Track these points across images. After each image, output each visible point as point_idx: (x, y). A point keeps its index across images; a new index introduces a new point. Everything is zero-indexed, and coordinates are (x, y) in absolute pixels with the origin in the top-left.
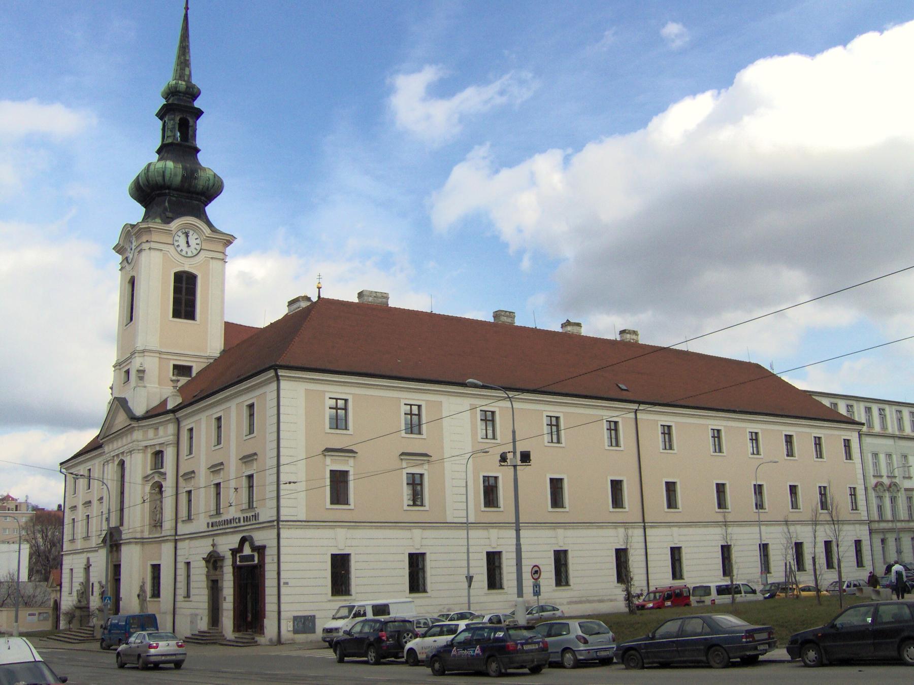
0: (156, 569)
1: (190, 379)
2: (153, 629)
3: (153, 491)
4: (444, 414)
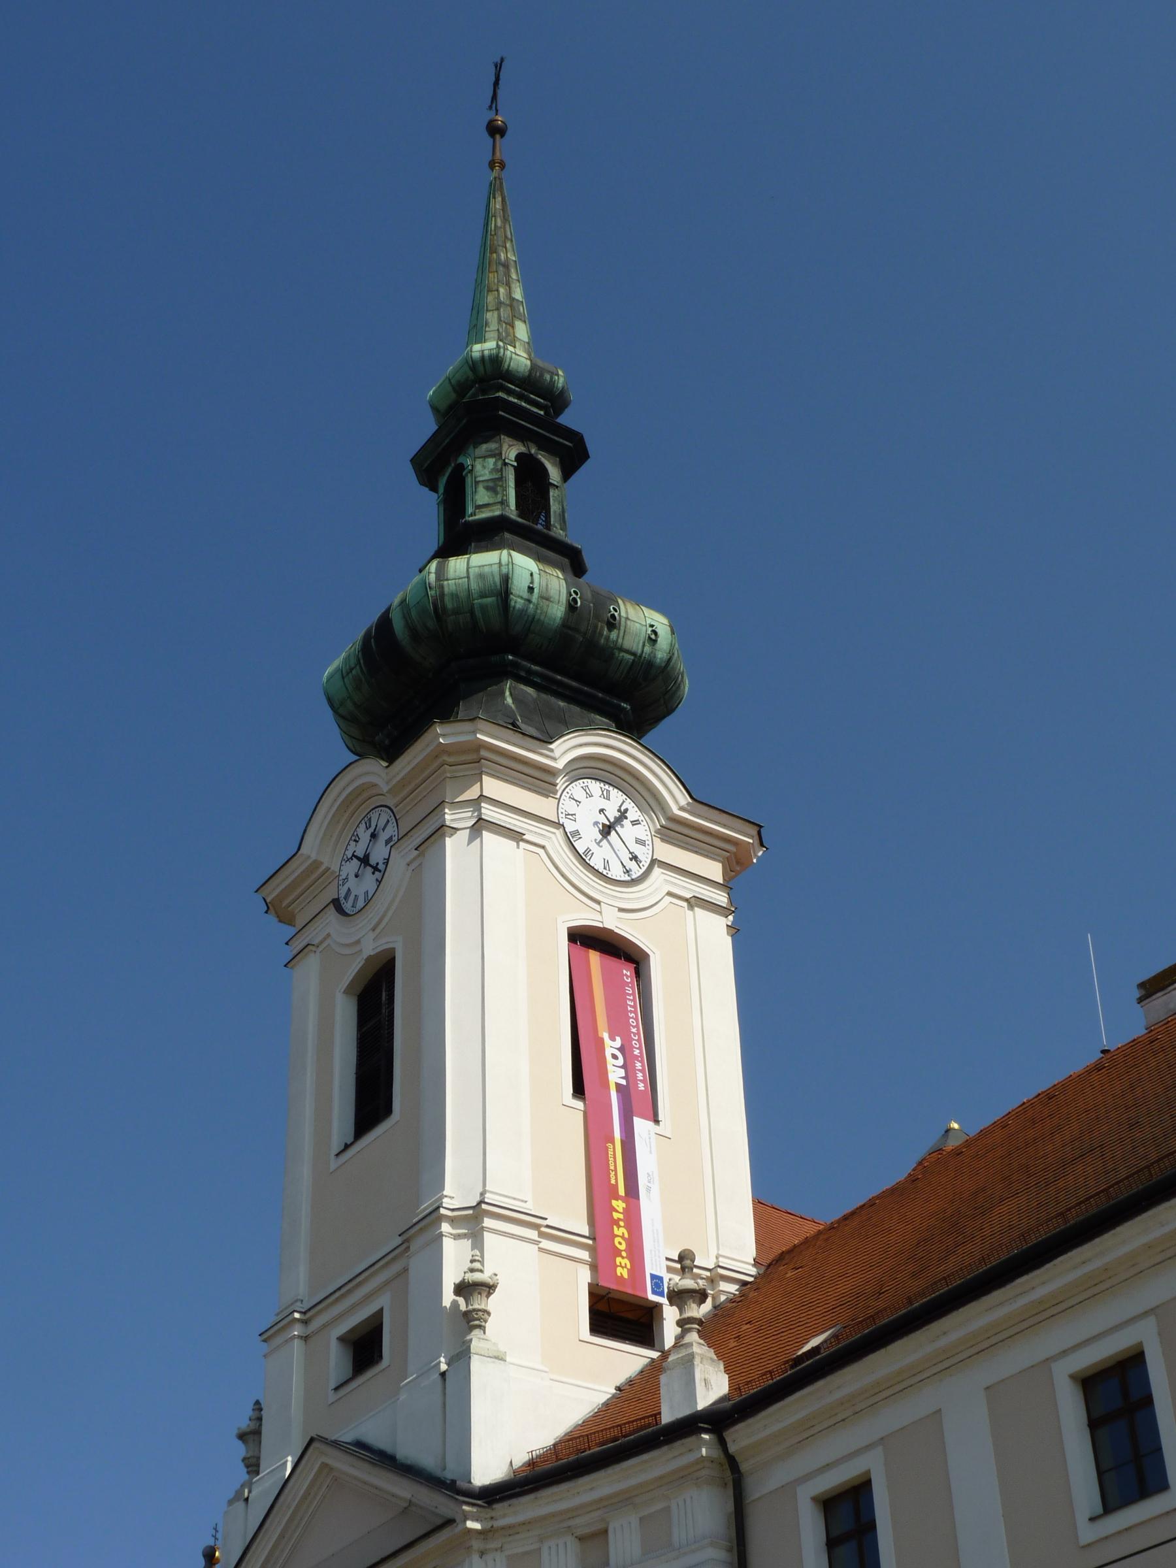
1: (655, 1355)
2: (469, 547)
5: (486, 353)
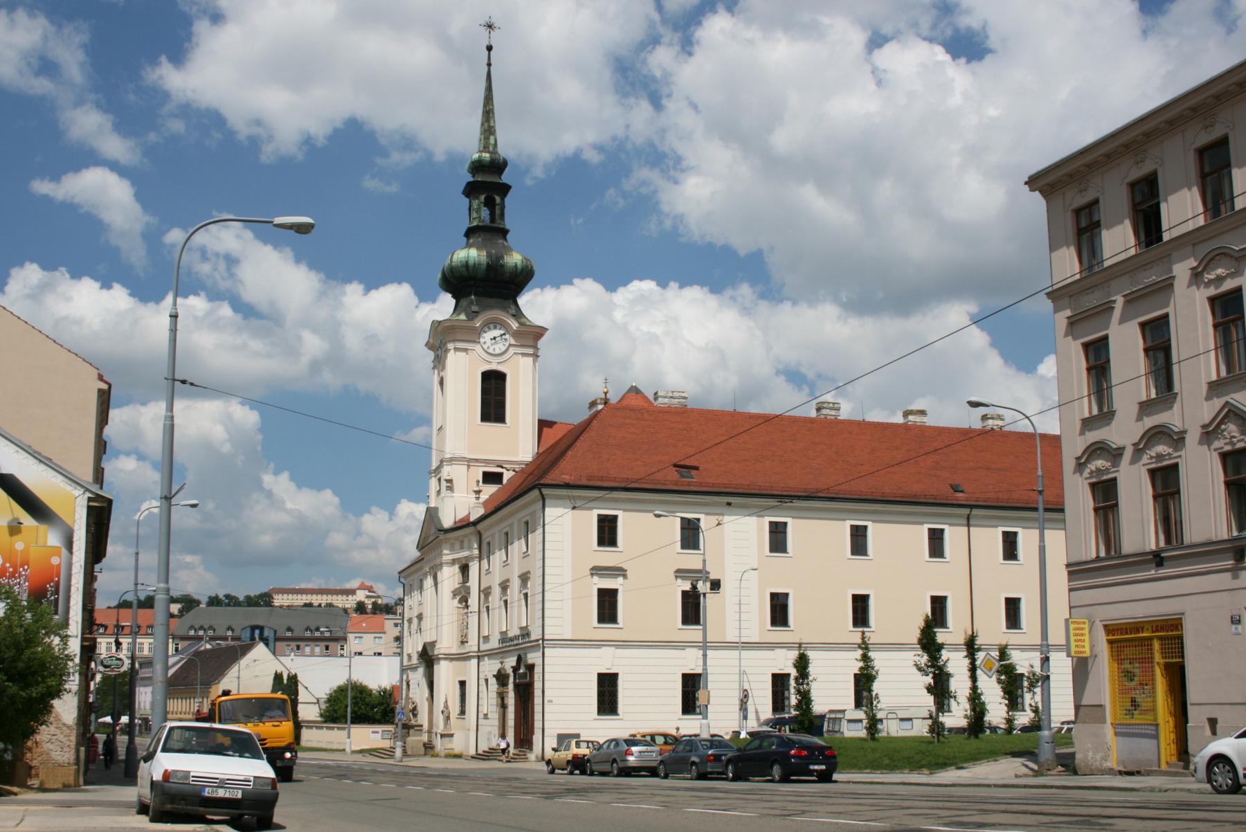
0: (463, 684)
1: (500, 486)
3: (460, 606)
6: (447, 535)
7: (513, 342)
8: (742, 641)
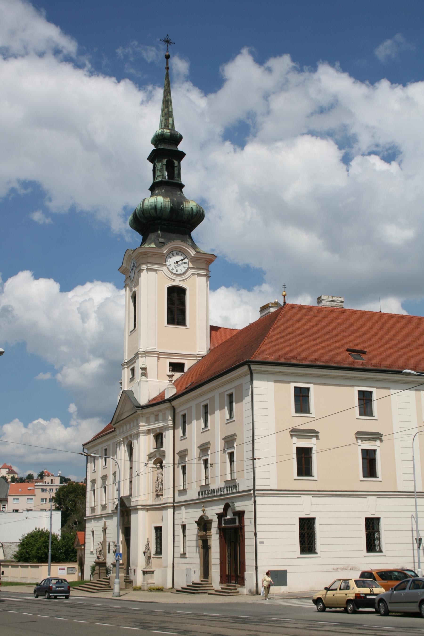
0: (158, 530)
1: (183, 373)
3: (155, 466)
4: (70, 595)
5: (159, 133)
6: (143, 410)
7: (191, 265)
8: (417, 491)
